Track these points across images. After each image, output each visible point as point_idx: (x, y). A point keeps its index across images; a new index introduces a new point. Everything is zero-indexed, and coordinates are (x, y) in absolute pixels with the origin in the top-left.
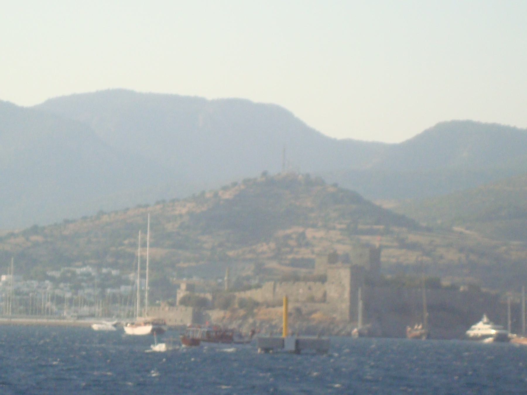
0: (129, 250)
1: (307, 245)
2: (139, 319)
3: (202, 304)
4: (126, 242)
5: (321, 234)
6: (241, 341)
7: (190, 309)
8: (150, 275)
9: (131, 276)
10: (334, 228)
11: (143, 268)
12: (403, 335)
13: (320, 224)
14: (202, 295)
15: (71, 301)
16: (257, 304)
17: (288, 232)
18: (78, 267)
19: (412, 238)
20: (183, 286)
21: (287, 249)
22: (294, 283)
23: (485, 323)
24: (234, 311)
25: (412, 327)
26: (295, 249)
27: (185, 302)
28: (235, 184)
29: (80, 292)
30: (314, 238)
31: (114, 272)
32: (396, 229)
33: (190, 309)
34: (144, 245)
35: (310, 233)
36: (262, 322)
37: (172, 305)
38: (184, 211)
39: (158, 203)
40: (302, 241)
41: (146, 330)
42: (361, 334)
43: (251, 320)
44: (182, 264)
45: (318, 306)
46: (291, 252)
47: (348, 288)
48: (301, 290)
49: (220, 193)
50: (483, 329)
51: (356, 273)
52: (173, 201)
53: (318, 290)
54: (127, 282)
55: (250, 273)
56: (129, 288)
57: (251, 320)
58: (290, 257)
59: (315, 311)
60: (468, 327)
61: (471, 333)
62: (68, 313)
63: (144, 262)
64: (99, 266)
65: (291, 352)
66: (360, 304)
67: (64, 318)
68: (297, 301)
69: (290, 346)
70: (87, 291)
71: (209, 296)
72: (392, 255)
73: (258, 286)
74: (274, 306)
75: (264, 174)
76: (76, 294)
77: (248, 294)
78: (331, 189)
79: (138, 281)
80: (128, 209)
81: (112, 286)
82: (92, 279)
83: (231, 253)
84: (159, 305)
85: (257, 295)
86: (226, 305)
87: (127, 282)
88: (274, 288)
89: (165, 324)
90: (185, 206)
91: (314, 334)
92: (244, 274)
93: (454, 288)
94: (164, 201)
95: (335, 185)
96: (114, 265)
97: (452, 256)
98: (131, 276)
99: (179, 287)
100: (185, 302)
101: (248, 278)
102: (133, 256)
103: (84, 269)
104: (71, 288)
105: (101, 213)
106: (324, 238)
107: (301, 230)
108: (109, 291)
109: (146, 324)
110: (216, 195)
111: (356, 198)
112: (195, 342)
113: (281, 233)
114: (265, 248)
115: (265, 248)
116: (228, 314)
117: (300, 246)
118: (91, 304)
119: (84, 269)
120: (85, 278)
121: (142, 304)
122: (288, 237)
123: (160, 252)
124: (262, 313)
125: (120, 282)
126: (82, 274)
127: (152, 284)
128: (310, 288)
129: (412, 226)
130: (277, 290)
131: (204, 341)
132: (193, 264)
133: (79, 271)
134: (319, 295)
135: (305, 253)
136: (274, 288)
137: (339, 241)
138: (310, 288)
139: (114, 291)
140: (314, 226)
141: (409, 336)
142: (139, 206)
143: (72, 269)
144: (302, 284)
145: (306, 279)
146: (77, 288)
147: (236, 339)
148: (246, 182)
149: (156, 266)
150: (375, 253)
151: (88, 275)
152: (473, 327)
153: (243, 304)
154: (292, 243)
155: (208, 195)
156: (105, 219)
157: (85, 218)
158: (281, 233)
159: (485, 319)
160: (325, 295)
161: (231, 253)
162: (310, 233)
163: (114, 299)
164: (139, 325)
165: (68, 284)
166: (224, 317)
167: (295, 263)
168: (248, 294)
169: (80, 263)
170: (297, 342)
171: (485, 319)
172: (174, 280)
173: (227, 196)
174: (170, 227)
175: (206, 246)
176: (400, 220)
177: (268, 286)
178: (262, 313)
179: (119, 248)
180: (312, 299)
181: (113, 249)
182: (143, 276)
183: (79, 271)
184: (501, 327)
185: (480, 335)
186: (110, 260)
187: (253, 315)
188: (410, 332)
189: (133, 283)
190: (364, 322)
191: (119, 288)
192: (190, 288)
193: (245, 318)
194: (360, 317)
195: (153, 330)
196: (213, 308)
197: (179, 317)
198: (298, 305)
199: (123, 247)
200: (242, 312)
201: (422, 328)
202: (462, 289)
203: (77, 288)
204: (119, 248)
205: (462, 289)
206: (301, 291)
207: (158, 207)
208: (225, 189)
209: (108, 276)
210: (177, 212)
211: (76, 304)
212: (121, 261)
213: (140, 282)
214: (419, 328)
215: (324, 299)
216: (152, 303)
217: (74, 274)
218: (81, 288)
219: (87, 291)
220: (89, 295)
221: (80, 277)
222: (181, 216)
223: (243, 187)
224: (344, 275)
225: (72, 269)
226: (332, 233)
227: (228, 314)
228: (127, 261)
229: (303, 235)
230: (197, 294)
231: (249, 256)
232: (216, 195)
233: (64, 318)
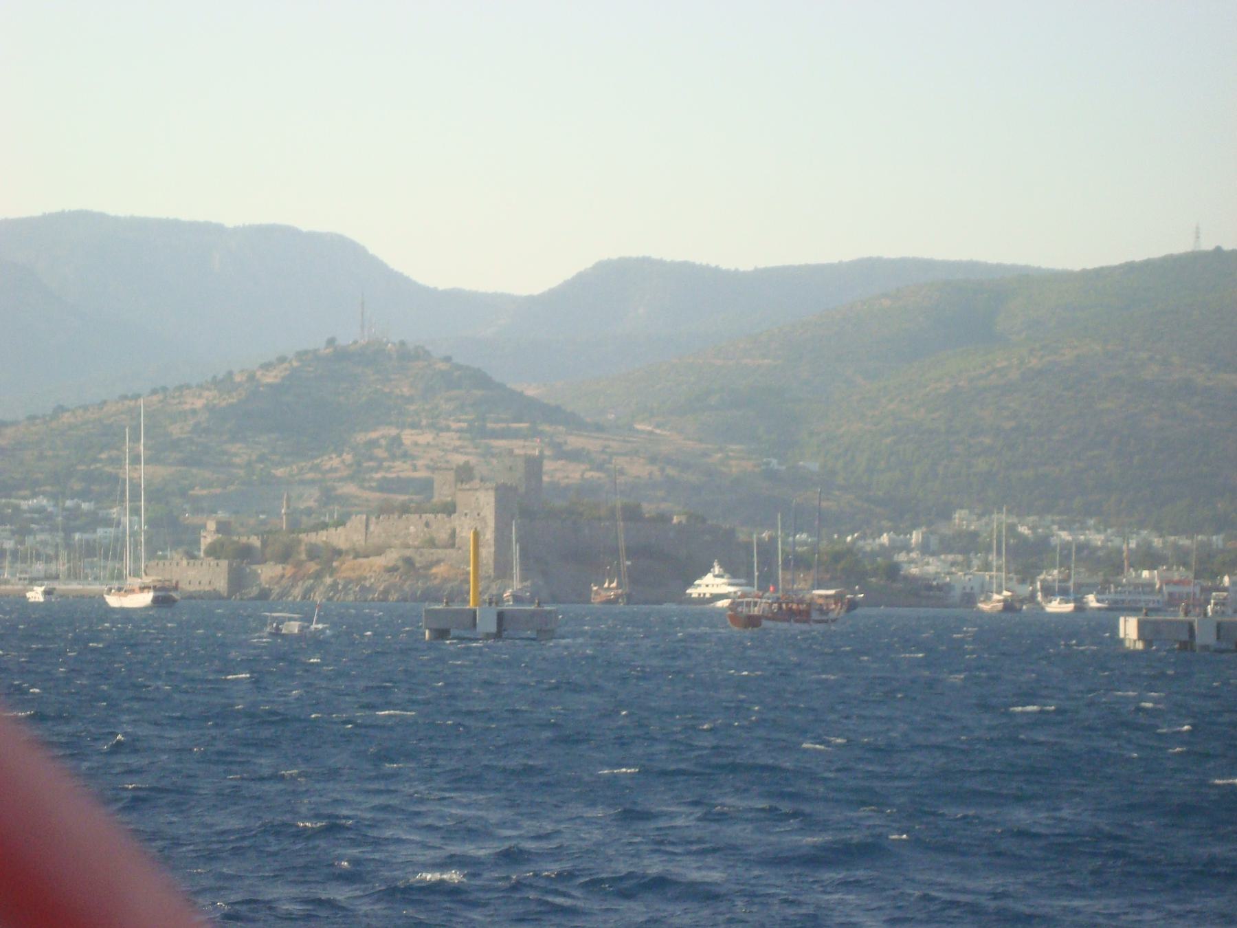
0: (108, 469)
1: (405, 456)
2: (134, 582)
3: (245, 553)
4: (103, 456)
5: (427, 438)
6: (824, 618)
7: (224, 564)
8: (146, 510)
9: (114, 512)
10: (448, 429)
11: (135, 497)
12: (583, 597)
13: (424, 422)
14: (244, 539)
15: (14, 553)
16: (338, 553)
17: (373, 435)
18: (25, 498)
19: (575, 442)
20: (212, 526)
21: (371, 464)
22: (400, 517)
23: (716, 576)
24: (299, 565)
25: (601, 585)
26: (386, 464)
27: (215, 551)
28: (282, 360)
29: (29, 540)
30: (416, 444)
31: (85, 506)
32: (546, 428)
33: (224, 564)
34: (136, 460)
35: (408, 437)
36: (349, 581)
37: (191, 556)
38: (199, 404)
39: (154, 392)
40: (396, 448)
41: (143, 600)
42: (517, 599)
43: (328, 580)
44: (197, 492)
45: (440, 553)
46: (379, 468)
47: (491, 523)
48: (413, 527)
49: (259, 374)
50: (713, 585)
51: (504, 495)
52: (180, 388)
53: (441, 527)
54: (108, 522)
55: (311, 503)
56: (111, 531)
57: (328, 580)
58: (378, 476)
59: (438, 562)
60: (690, 584)
61: (693, 592)
62: (14, 575)
63: (135, 488)
64: (54, 497)
65: (488, 636)
66: (516, 549)
67: (6, 582)
68: (407, 546)
69: (487, 624)
70: (40, 537)
71: (256, 542)
72: (556, 472)
73: (341, 523)
74: (367, 556)
75: (331, 342)
76: (22, 543)
77: (321, 537)
78: (443, 366)
79: (126, 520)
80: (104, 402)
81: (81, 529)
82: (49, 517)
83: (280, 472)
84: (164, 557)
85: (338, 537)
86: (285, 556)
87: (108, 522)
88: (367, 526)
89: (176, 588)
90: (200, 396)
91: (437, 600)
92: (302, 506)
93: (663, 518)
94: (165, 389)
95: (448, 359)
96: (84, 495)
97: (638, 470)
98: (114, 512)
99: (204, 526)
100: (215, 551)
101: (309, 512)
102: (115, 479)
103: (34, 502)
104: (13, 533)
105: (60, 409)
106: (431, 446)
107: (393, 432)
108: (77, 536)
109: (143, 589)
110: (252, 378)
111: (481, 380)
112: (753, 621)
113: (361, 438)
114: (336, 462)
115: (336, 462)
116: (290, 570)
117: (393, 457)
118: (49, 559)
119: (34, 502)
120: (36, 516)
121: (137, 559)
122: (373, 443)
123: (163, 472)
124: (347, 568)
125: (96, 521)
126: (32, 510)
127: (151, 523)
128: (427, 525)
129: (574, 423)
130: (372, 528)
131: (768, 618)
132: (218, 491)
133: (24, 505)
134: (443, 536)
135: (402, 470)
136: (367, 526)
137: (456, 450)
138: (427, 525)
139: (86, 536)
140: (413, 426)
141: (596, 599)
142: (125, 397)
143: (13, 501)
144: (414, 517)
145: (420, 510)
146: (22, 532)
147: (815, 616)
148: (300, 355)
149: (157, 495)
150: (534, 466)
151: (41, 510)
152: (697, 582)
153: (314, 553)
154: (380, 453)
155: (238, 378)
156: (66, 418)
157: (32, 418)
158: (361, 438)
159: (717, 570)
160: (453, 534)
161: (280, 472)
162: (408, 437)
163: (90, 550)
164: (132, 591)
165: (8, 527)
166: (283, 576)
167: (385, 486)
168: (321, 537)
169: (27, 493)
170: (501, 617)
171: (717, 570)
172: (188, 518)
173: (270, 378)
174: (176, 430)
175: (237, 460)
176: (553, 414)
177: (357, 521)
178: (347, 568)
179: (92, 467)
180: (432, 543)
181: (82, 467)
182: (135, 511)
183: (24, 505)
184: (742, 581)
185: (708, 596)
186: (78, 486)
187: (333, 572)
188: (597, 593)
189: (119, 524)
190: (524, 579)
191: (95, 531)
192: (223, 528)
193: (318, 576)
194: (516, 571)
195: (156, 600)
196: (263, 561)
197: (202, 576)
198: (408, 553)
199: (99, 465)
200: (313, 567)
201: (619, 586)
202: (675, 520)
203: (22, 532)
204: (92, 467)
205: (675, 520)
206: (412, 529)
207: (155, 398)
208: (267, 366)
209: (74, 514)
210: (187, 407)
211: (24, 560)
212: (96, 488)
213: (130, 521)
214: (611, 588)
215: (452, 543)
216: (152, 555)
217: (17, 508)
218: (31, 532)
219: (40, 537)
220: (44, 543)
221: (28, 515)
222: (194, 412)
223: (295, 364)
224: (486, 501)
225: (13, 501)
226: (446, 437)
227: (290, 570)
228: (108, 487)
229: (397, 441)
230: (235, 538)
231: (310, 476)
232: (252, 378)
233: (6, 582)
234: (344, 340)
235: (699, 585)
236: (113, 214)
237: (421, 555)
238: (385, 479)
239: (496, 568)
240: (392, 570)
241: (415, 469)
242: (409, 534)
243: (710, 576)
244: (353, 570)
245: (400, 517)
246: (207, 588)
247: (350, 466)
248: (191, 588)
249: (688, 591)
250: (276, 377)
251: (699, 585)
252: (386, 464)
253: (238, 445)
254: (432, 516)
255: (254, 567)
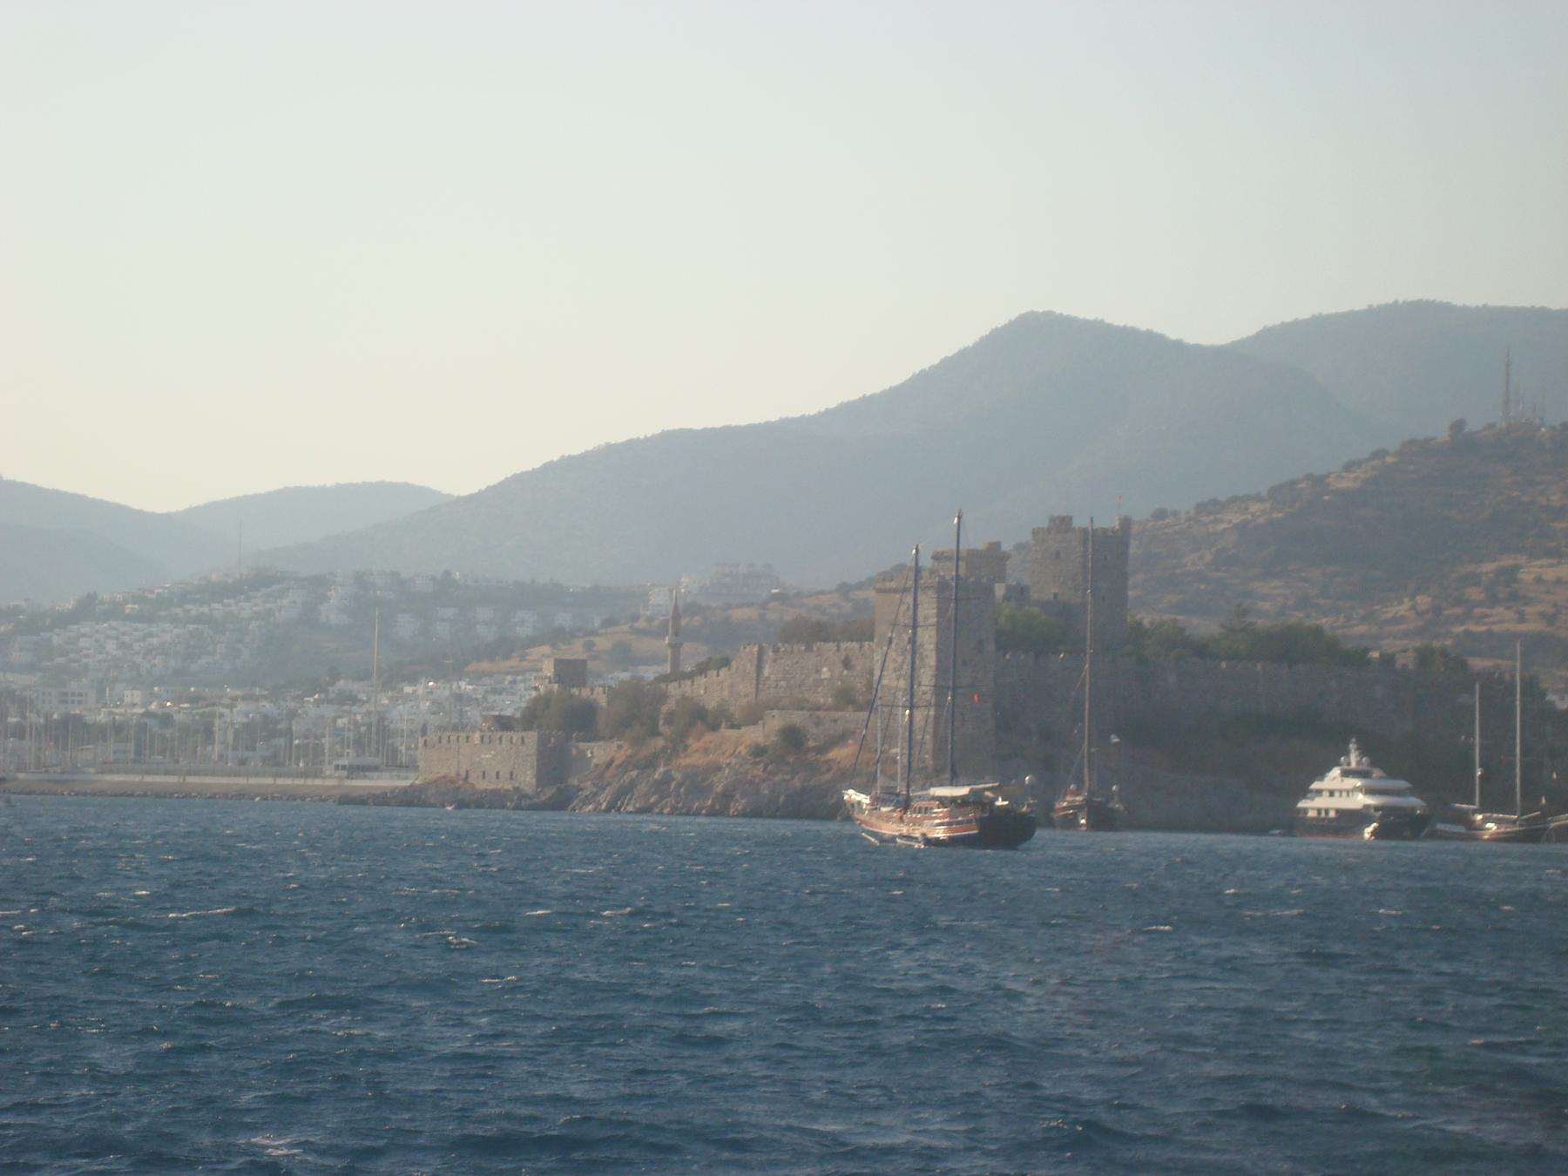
21: (1458, 611)
30: (1539, 580)
58: (1458, 629)
59: (840, 739)
60: (1304, 792)
61: (1311, 806)
117: (1493, 601)
128: (847, 663)
130: (766, 672)
136: (759, 668)
138: (847, 663)
152: (1315, 785)
154: (1475, 594)
159: (1353, 759)
171: (1353, 759)
198: (797, 718)
229: (1510, 574)
234: (1474, 425)
235: (1319, 792)
236: (1460, 304)
237: (818, 723)
238: (1467, 632)
239: (938, 751)
240: (758, 751)
241: (1522, 618)
242: (818, 683)
243: (1336, 771)
244: (706, 751)
245: (809, 649)
246: (508, 786)
247: (1420, 614)
248: (482, 785)
249: (1301, 804)
250: (1356, 479)
251: (1319, 792)
252: (1478, 611)
253: (1275, 583)
254: (855, 645)
255: (582, 745)
